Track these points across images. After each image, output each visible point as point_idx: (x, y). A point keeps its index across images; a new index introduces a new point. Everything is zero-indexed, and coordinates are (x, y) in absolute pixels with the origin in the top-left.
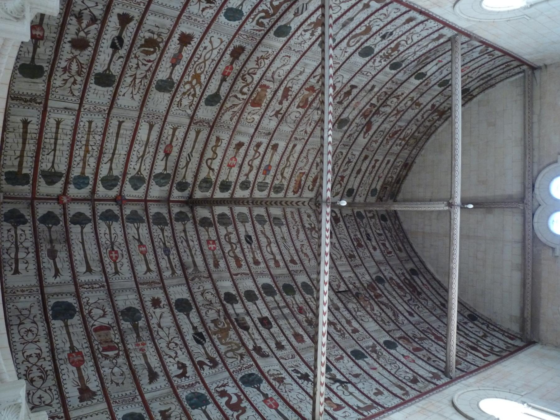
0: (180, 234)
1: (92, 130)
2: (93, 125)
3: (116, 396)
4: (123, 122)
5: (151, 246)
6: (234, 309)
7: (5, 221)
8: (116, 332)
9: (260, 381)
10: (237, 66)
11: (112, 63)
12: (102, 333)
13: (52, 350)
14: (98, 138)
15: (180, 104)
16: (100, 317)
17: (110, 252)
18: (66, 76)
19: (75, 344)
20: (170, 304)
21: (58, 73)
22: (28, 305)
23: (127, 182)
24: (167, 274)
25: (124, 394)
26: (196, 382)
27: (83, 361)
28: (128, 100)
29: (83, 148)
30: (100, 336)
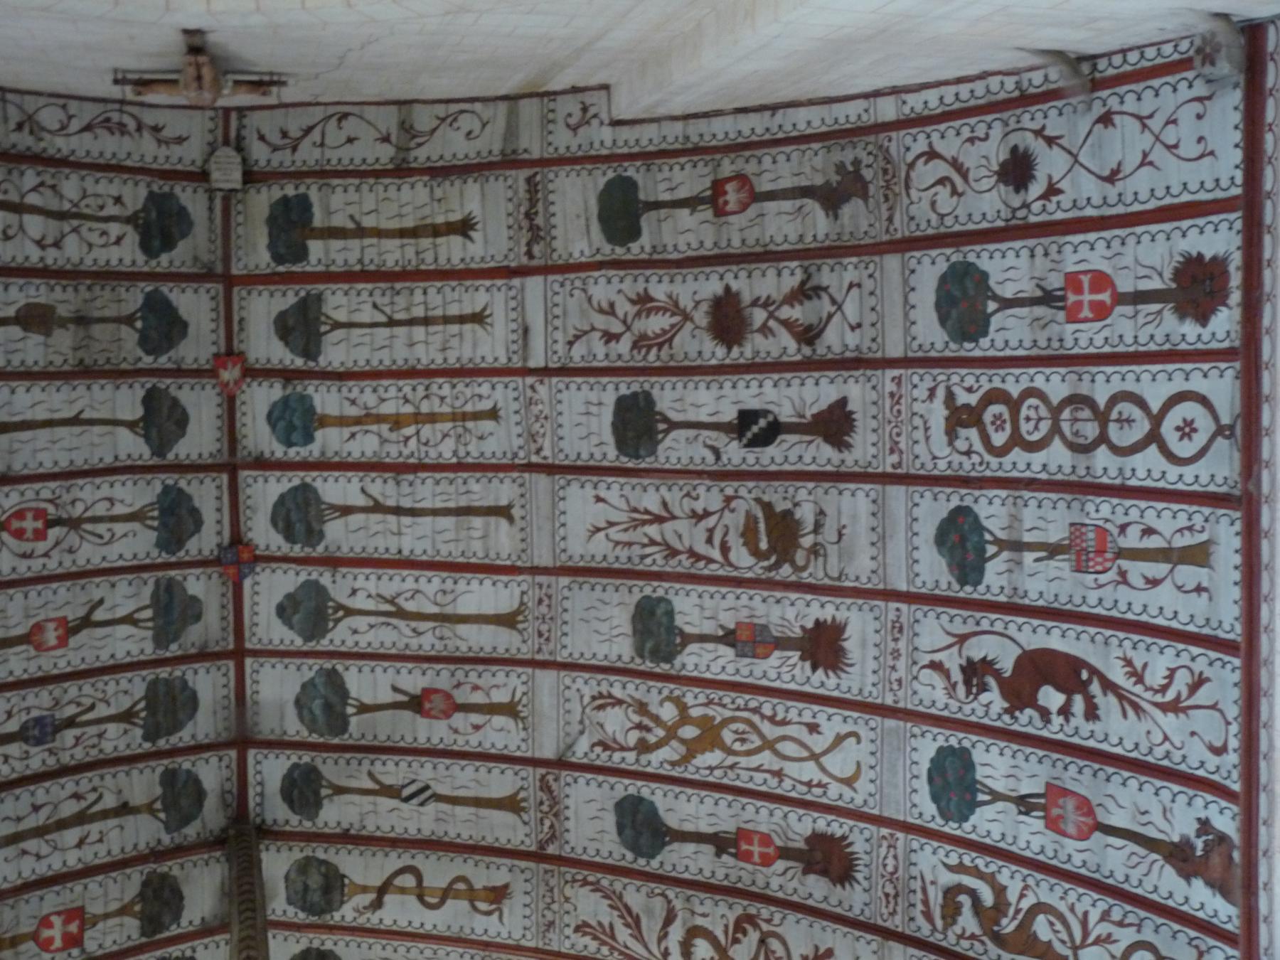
1: (470, 425)
2: (487, 425)
4: (511, 519)
5: (63, 667)
7: (151, 194)
10: (781, 878)
11: (691, 433)
14: (446, 450)
15: (605, 701)
17: (39, 514)
18: (624, 307)
21: (631, 285)
23: (303, 577)
28: (585, 518)
29: (408, 409)
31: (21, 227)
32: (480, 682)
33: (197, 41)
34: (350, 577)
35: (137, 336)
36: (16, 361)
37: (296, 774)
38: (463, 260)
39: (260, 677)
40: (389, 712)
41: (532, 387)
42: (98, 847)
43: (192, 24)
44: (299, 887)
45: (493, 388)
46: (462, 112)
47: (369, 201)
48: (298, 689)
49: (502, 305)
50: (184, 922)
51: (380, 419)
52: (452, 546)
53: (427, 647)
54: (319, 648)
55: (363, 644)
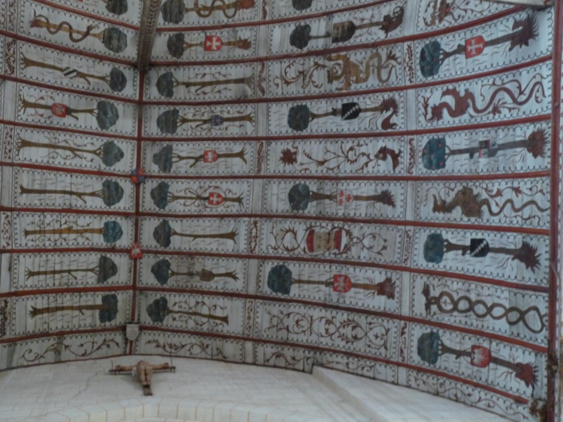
0: (191, 94)
1: (38, 229)
2: (30, 228)
3: (399, 256)
4: (22, 188)
5: (207, 143)
6: (317, 37)
8: (318, 224)
9: (436, 46)
12: (316, 242)
13: (324, 306)
14: (49, 218)
16: (295, 238)
17: (211, 203)
19: (324, 278)
20: (294, 138)
22: (267, 317)
23: (112, 168)
24: (249, 129)
25: (398, 245)
26: (410, 143)
27: (346, 278)
29: (64, 236)
30: (319, 247)
31: (210, 310)
32: (39, 118)
33: (147, 390)
34: (93, 167)
35: (171, 267)
36: (215, 260)
37: (120, 87)
38: (37, 298)
39: (132, 129)
40: (80, 108)
41: (8, 244)
42: (198, 72)
43: (149, 398)
44: (121, 41)
45: (26, 245)
46: (33, 361)
47: (75, 322)
48: (117, 122)
49: (20, 276)
50: (167, 36)
51: (77, 232)
52: (49, 177)
53: (62, 135)
54: (107, 138)
55: (89, 138)
